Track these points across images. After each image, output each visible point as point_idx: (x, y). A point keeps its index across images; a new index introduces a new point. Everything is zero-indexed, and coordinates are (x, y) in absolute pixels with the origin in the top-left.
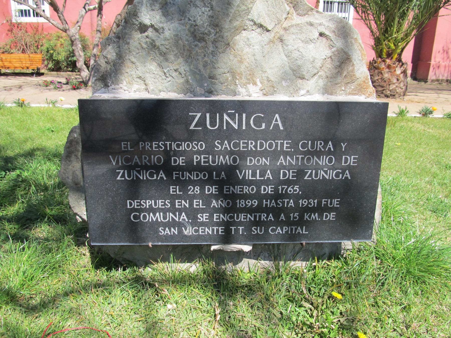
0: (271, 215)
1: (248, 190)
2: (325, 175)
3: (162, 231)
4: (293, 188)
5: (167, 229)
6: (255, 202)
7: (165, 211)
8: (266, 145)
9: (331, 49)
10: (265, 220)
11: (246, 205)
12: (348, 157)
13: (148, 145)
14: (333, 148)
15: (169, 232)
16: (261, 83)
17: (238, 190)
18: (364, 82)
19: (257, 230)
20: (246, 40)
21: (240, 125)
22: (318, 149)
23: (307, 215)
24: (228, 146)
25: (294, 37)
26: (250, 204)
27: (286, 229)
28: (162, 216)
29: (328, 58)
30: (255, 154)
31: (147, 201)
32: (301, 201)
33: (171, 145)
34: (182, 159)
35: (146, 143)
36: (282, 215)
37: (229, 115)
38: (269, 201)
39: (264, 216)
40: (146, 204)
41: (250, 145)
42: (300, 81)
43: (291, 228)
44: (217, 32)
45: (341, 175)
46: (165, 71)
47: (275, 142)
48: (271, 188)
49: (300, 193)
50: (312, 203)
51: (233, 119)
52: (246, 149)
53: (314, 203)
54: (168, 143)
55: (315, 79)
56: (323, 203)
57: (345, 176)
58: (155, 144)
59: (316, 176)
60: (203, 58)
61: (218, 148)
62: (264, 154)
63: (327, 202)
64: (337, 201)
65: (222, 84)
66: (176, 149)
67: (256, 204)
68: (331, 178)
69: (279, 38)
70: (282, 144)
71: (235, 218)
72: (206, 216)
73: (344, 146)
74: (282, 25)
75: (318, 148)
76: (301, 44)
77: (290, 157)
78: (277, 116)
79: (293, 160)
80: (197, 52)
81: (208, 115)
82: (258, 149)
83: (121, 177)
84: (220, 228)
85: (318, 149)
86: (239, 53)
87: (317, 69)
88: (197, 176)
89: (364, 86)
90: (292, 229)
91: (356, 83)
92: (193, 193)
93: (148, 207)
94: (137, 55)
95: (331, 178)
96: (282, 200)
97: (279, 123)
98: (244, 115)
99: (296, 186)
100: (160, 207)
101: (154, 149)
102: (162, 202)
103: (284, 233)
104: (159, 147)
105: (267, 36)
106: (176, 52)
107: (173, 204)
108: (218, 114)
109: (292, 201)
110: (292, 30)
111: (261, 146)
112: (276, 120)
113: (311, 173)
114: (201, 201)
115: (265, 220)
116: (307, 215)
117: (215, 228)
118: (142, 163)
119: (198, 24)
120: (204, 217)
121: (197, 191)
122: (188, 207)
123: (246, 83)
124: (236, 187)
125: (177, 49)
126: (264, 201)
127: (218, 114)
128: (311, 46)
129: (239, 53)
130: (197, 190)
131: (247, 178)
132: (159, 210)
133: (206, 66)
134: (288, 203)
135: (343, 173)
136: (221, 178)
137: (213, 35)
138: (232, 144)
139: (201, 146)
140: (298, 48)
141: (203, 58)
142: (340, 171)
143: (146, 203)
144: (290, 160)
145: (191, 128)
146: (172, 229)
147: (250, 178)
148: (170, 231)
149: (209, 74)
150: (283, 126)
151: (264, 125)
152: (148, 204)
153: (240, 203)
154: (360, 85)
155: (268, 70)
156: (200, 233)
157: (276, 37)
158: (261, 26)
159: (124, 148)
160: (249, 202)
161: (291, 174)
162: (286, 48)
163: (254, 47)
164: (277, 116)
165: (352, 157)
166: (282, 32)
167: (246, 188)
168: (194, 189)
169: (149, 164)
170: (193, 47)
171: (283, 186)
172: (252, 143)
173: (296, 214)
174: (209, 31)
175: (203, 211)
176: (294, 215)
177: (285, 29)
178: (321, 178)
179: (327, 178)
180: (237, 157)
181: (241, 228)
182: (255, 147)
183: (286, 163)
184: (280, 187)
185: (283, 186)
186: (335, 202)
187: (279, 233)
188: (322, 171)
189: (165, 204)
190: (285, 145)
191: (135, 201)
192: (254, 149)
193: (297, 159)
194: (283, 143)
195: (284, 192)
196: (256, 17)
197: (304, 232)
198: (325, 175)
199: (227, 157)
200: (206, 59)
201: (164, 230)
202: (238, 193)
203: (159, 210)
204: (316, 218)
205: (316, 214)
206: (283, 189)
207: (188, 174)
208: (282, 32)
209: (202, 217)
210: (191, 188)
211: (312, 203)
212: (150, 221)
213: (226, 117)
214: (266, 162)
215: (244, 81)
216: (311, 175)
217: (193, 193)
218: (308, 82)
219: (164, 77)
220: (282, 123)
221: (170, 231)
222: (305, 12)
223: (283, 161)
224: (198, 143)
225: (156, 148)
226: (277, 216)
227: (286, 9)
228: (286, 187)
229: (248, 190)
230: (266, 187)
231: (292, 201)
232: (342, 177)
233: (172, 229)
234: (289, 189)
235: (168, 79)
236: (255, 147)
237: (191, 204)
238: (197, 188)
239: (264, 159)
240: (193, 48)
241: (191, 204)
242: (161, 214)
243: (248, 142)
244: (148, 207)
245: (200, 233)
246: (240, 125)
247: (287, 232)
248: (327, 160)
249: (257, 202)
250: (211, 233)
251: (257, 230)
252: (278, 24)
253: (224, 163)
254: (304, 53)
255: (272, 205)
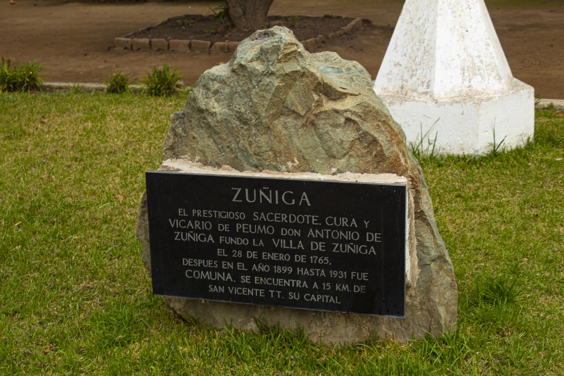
0: (305, 282)
1: (284, 258)
2: (351, 249)
3: (211, 288)
4: (323, 259)
5: (215, 287)
6: (290, 269)
7: (213, 270)
8: (297, 219)
9: (359, 131)
10: (300, 286)
11: (283, 271)
12: (372, 234)
13: (199, 212)
14: (357, 224)
15: (216, 290)
16: (298, 160)
17: (275, 257)
18: (396, 160)
19: (293, 295)
20: (283, 124)
21: (274, 200)
22: (343, 225)
23: (338, 286)
24: (264, 217)
25: (323, 122)
26: (286, 271)
27: (319, 297)
28: (211, 275)
29: (356, 140)
30: (288, 226)
31: (199, 260)
32: (331, 272)
33: (217, 213)
34: (227, 226)
35: (198, 211)
36: (315, 283)
37: (264, 191)
38: (302, 269)
39: (299, 282)
40: (198, 263)
41: (283, 218)
42: (332, 160)
43: (324, 297)
44: (257, 119)
45: (366, 251)
46: (220, 147)
47: (304, 217)
48: (304, 257)
49: (330, 264)
50: (342, 274)
51: (268, 195)
52: (248, 232)
53: (344, 275)
54: (215, 212)
55: (346, 158)
56: (352, 275)
57: (370, 251)
58: (205, 212)
59: (344, 249)
60: (248, 138)
61: (256, 218)
62: (295, 226)
63: (356, 274)
64: (366, 275)
65: (265, 160)
66: (222, 217)
67: (291, 271)
68: (357, 253)
69: (310, 122)
70: (310, 219)
71: (273, 282)
72: (248, 278)
73: (366, 224)
74: (312, 112)
75: (343, 224)
76: (330, 128)
77: (318, 230)
78: (304, 194)
79: (321, 234)
80: (243, 133)
81: (247, 190)
82: (290, 222)
83: (178, 238)
84: (260, 290)
85: (343, 225)
86: (279, 134)
87: (346, 150)
88: (240, 241)
89: (396, 164)
90: (325, 298)
91: (387, 161)
92: (236, 256)
93: (199, 266)
94: (198, 132)
95: (357, 253)
96: (314, 269)
97: (307, 200)
98: (277, 192)
99: (325, 258)
100: (209, 266)
101: (204, 216)
102: (211, 262)
103: (318, 300)
104: (208, 214)
105: (300, 122)
106: (227, 132)
107: (220, 265)
108: (255, 190)
109: (323, 271)
110: (322, 116)
111: (293, 219)
112: (304, 198)
113: (339, 246)
114: (243, 264)
115: (300, 286)
116: (338, 286)
117: (256, 290)
118: (194, 227)
119: (242, 111)
120: (247, 279)
121: (240, 255)
122: (232, 268)
123: (286, 160)
124: (273, 254)
125: (227, 130)
126: (298, 268)
127: (255, 190)
128: (338, 130)
129: (279, 134)
130: (240, 253)
131: (282, 247)
132: (208, 269)
133: (251, 145)
134: (320, 272)
135: (369, 249)
136: (259, 245)
137: (254, 120)
138: (267, 216)
139: (242, 216)
140: (327, 131)
141: (248, 138)
142: (366, 246)
143: (197, 262)
144: (319, 233)
145: (233, 200)
146: (220, 288)
147: (285, 247)
148: (218, 289)
149: (254, 152)
150: (310, 202)
151: (293, 201)
152: (199, 263)
153: (277, 269)
154: (391, 163)
155: (303, 150)
156: (244, 294)
157: (308, 122)
158: (294, 112)
159: (181, 213)
160: (284, 269)
161: (320, 246)
162: (318, 131)
163: (291, 130)
164: (304, 194)
165: (376, 234)
166: (313, 118)
167: (282, 256)
168: (237, 253)
169: (200, 228)
170: (240, 129)
171: (314, 257)
172: (284, 216)
173: (328, 284)
174: (251, 118)
175: (245, 273)
176: (326, 285)
177: (315, 115)
178: (348, 252)
179: (354, 252)
180: (273, 228)
181: (279, 292)
182: (288, 219)
183: (315, 236)
184: (311, 257)
185: (314, 257)
186: (364, 276)
187: (313, 300)
188: (348, 246)
189: (213, 265)
190: (313, 220)
191: (189, 259)
192: (286, 221)
193: (325, 232)
194: (312, 217)
195: (315, 262)
196: (290, 105)
197: (337, 302)
198: (351, 249)
199: (264, 226)
200: (250, 139)
201: (213, 288)
202: (275, 259)
203: (208, 269)
204: (346, 289)
205: (347, 286)
206: (314, 259)
207: (232, 239)
208: (313, 118)
209: (245, 278)
210: (234, 252)
211: (342, 274)
212: (201, 278)
213: (261, 193)
214: (298, 233)
215: (283, 158)
216: (338, 248)
217: (236, 256)
218: (340, 160)
219: (219, 152)
220: (309, 200)
221: (218, 289)
222: (339, 97)
223: (312, 234)
224: (240, 213)
225: (205, 215)
226: (310, 284)
227: (314, 99)
228: (317, 257)
229: (284, 258)
230: (299, 257)
231: (323, 271)
232: (368, 252)
233: (220, 288)
234: (320, 260)
235: (223, 154)
236: (288, 219)
237: (235, 266)
238: (240, 252)
239: (295, 231)
240: (240, 130)
241: (235, 266)
242: (210, 272)
243: (281, 215)
244: (199, 266)
245: (244, 294)
246: (274, 200)
247: (321, 300)
248: (352, 235)
249: (291, 269)
250: (252, 294)
251: (293, 295)
252: (309, 111)
253: (261, 232)
254: (332, 136)
255: (305, 273)
